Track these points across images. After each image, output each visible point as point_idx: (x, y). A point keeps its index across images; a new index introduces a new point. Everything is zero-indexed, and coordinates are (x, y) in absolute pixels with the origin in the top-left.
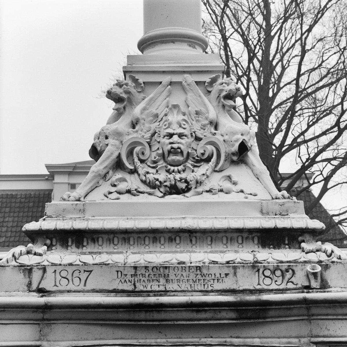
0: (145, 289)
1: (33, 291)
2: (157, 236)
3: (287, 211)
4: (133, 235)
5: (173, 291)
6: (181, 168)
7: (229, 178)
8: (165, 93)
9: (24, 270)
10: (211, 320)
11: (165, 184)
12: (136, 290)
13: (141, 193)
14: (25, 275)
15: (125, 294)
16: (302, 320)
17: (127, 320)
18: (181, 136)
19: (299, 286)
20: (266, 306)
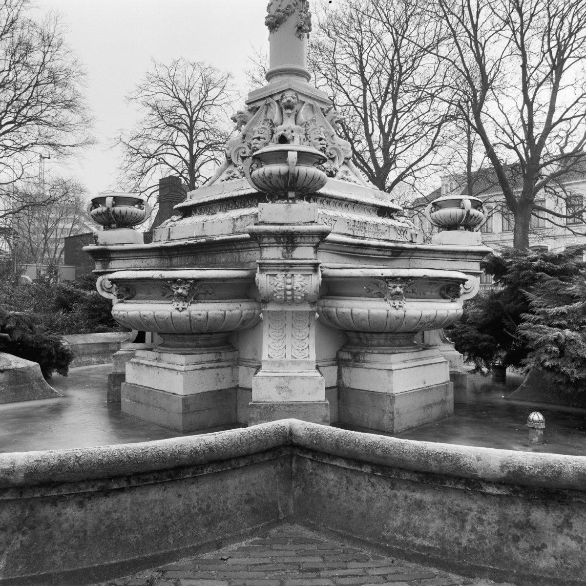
4: (333, 200)
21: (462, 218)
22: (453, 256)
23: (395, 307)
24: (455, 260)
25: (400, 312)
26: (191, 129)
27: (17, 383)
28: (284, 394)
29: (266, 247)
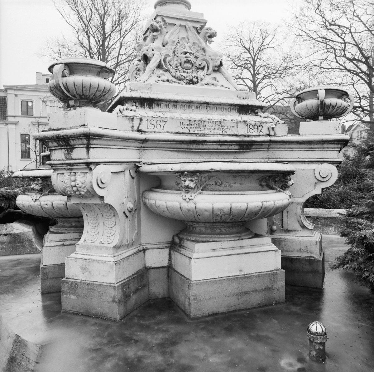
0: (194, 133)
1: (135, 131)
2: (191, 105)
3: (248, 97)
4: (179, 103)
5: (207, 134)
6: (191, 71)
7: (215, 78)
8: (178, 31)
9: (129, 119)
10: (226, 149)
11: (187, 78)
12: (190, 133)
13: (174, 82)
14: (130, 122)
15: (185, 135)
16: (265, 150)
17: (186, 149)
18: (190, 54)
19: (265, 134)
20: (252, 143)
21: (318, 109)
22: (309, 146)
23: (186, 200)
24: (312, 149)
25: (191, 205)
26: (254, 66)
27: (15, 242)
28: (86, 274)
29: (54, 150)
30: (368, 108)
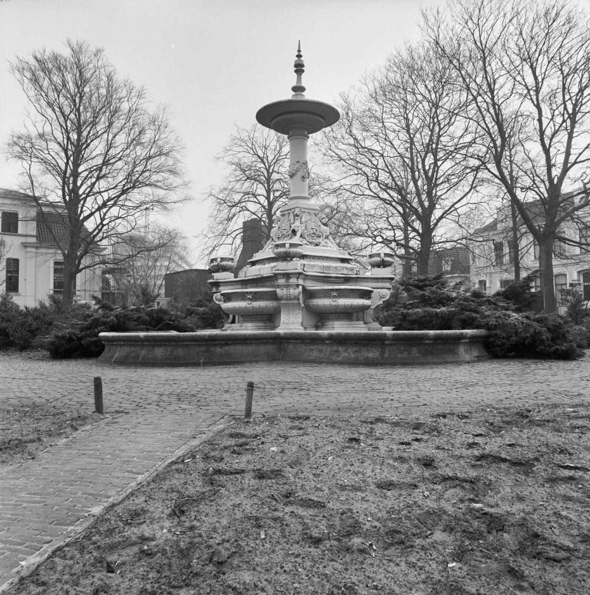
24: (378, 282)
25: (336, 303)
26: (268, 179)
30: (403, 242)
